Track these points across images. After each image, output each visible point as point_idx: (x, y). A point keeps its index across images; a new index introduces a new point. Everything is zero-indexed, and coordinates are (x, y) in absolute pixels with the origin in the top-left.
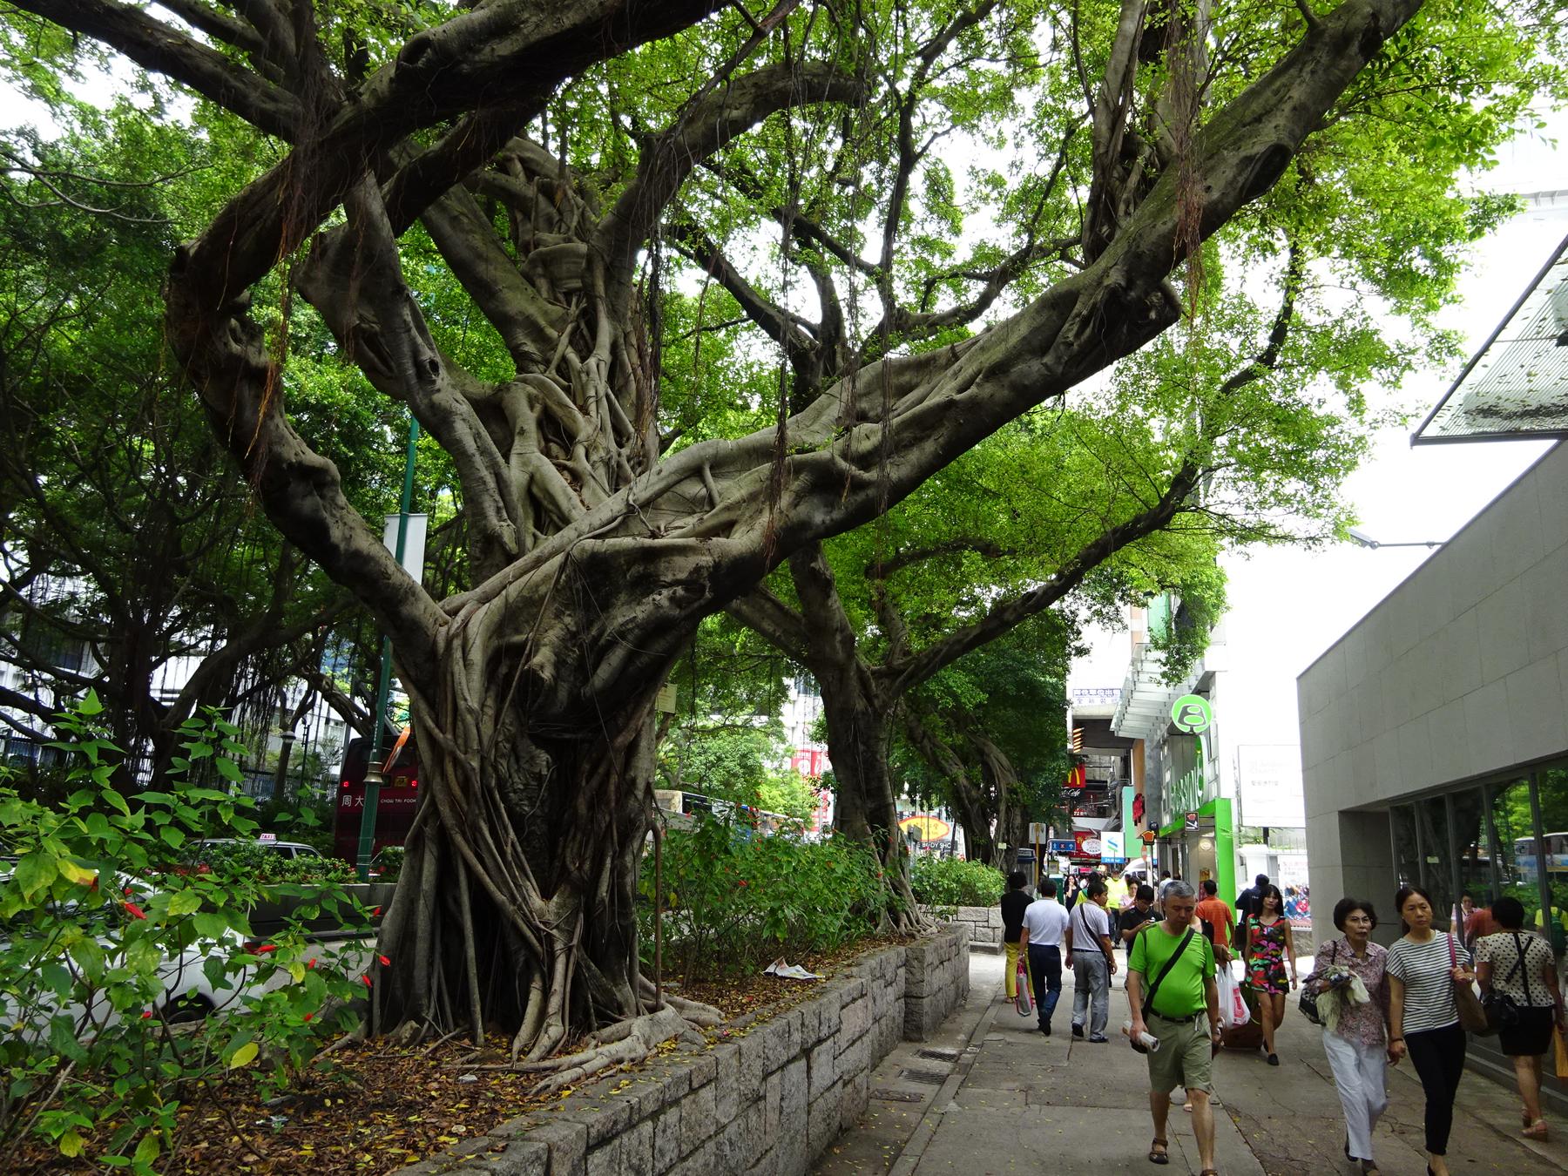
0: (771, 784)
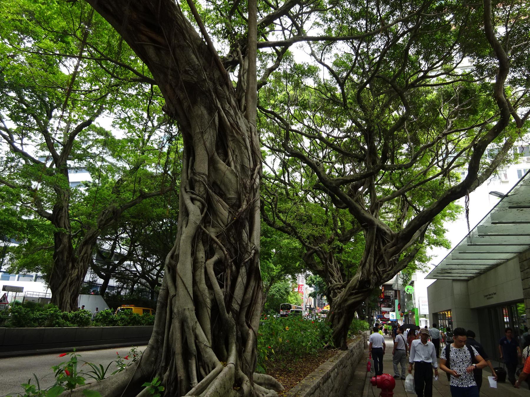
0: (291, 296)
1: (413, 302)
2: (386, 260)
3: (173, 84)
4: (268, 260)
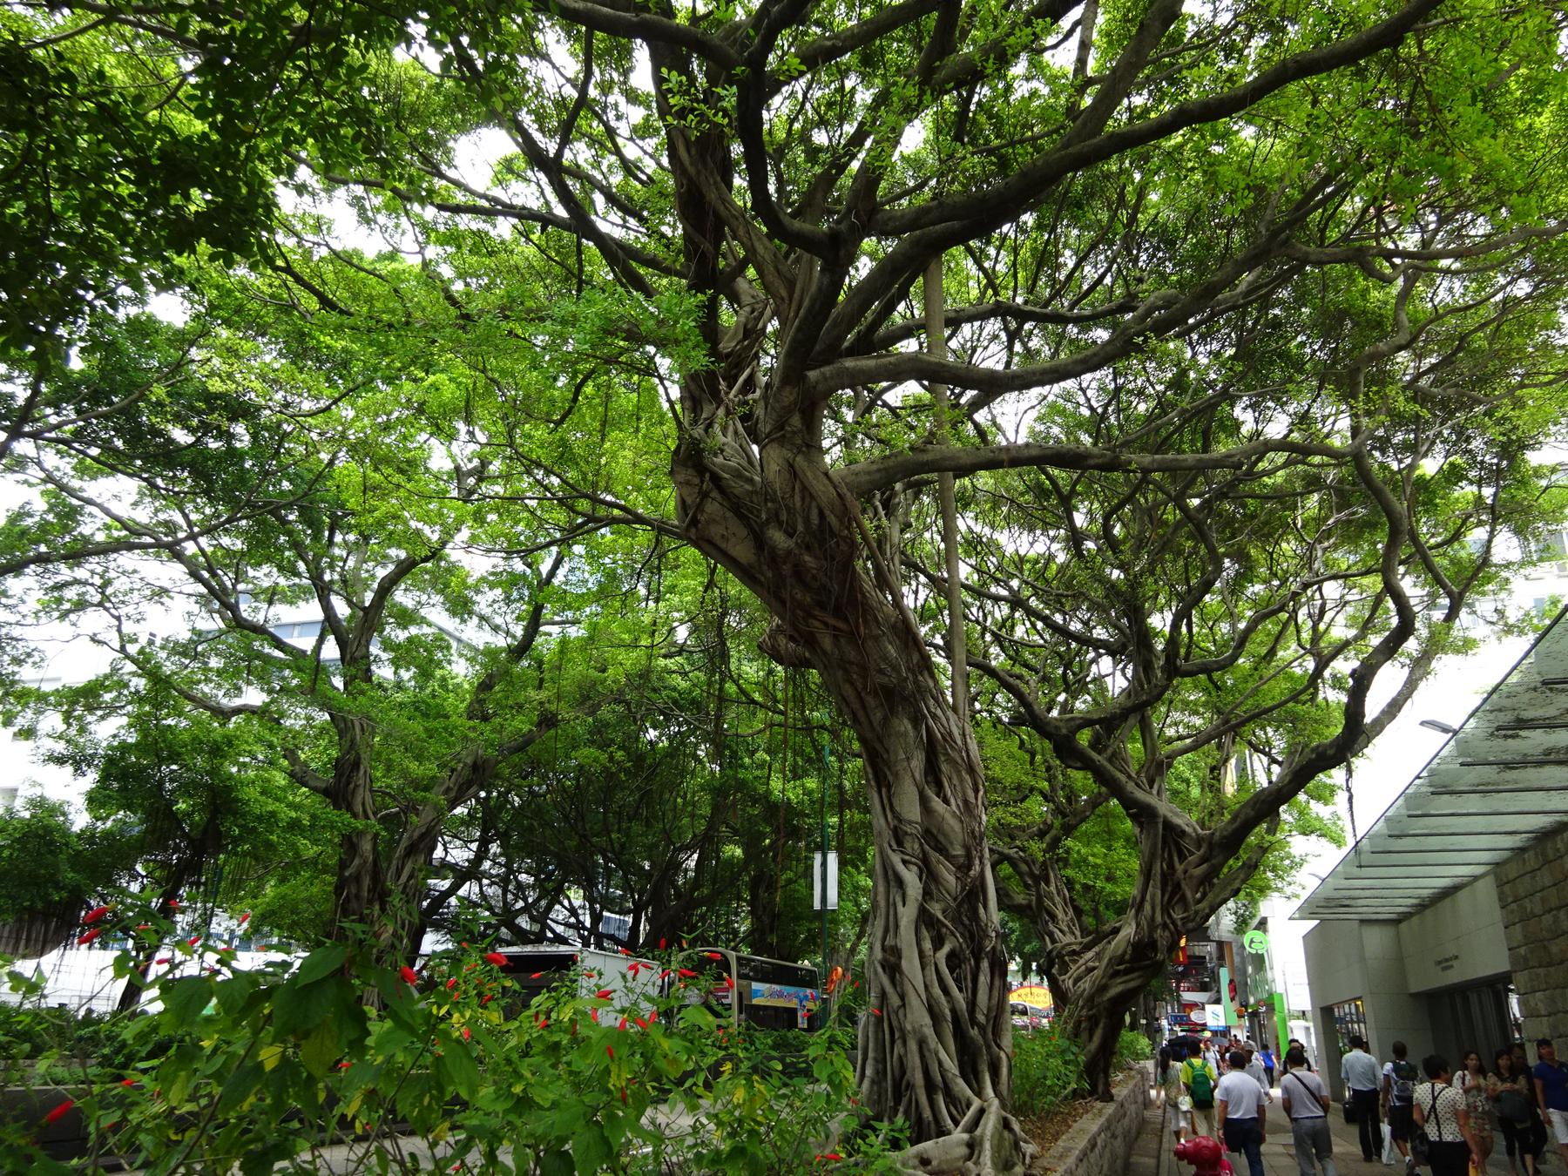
1: (1269, 975)
2: (1189, 894)
3: (859, 686)
4: (857, 868)
